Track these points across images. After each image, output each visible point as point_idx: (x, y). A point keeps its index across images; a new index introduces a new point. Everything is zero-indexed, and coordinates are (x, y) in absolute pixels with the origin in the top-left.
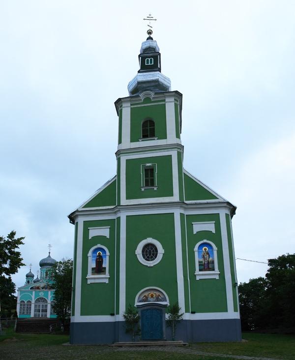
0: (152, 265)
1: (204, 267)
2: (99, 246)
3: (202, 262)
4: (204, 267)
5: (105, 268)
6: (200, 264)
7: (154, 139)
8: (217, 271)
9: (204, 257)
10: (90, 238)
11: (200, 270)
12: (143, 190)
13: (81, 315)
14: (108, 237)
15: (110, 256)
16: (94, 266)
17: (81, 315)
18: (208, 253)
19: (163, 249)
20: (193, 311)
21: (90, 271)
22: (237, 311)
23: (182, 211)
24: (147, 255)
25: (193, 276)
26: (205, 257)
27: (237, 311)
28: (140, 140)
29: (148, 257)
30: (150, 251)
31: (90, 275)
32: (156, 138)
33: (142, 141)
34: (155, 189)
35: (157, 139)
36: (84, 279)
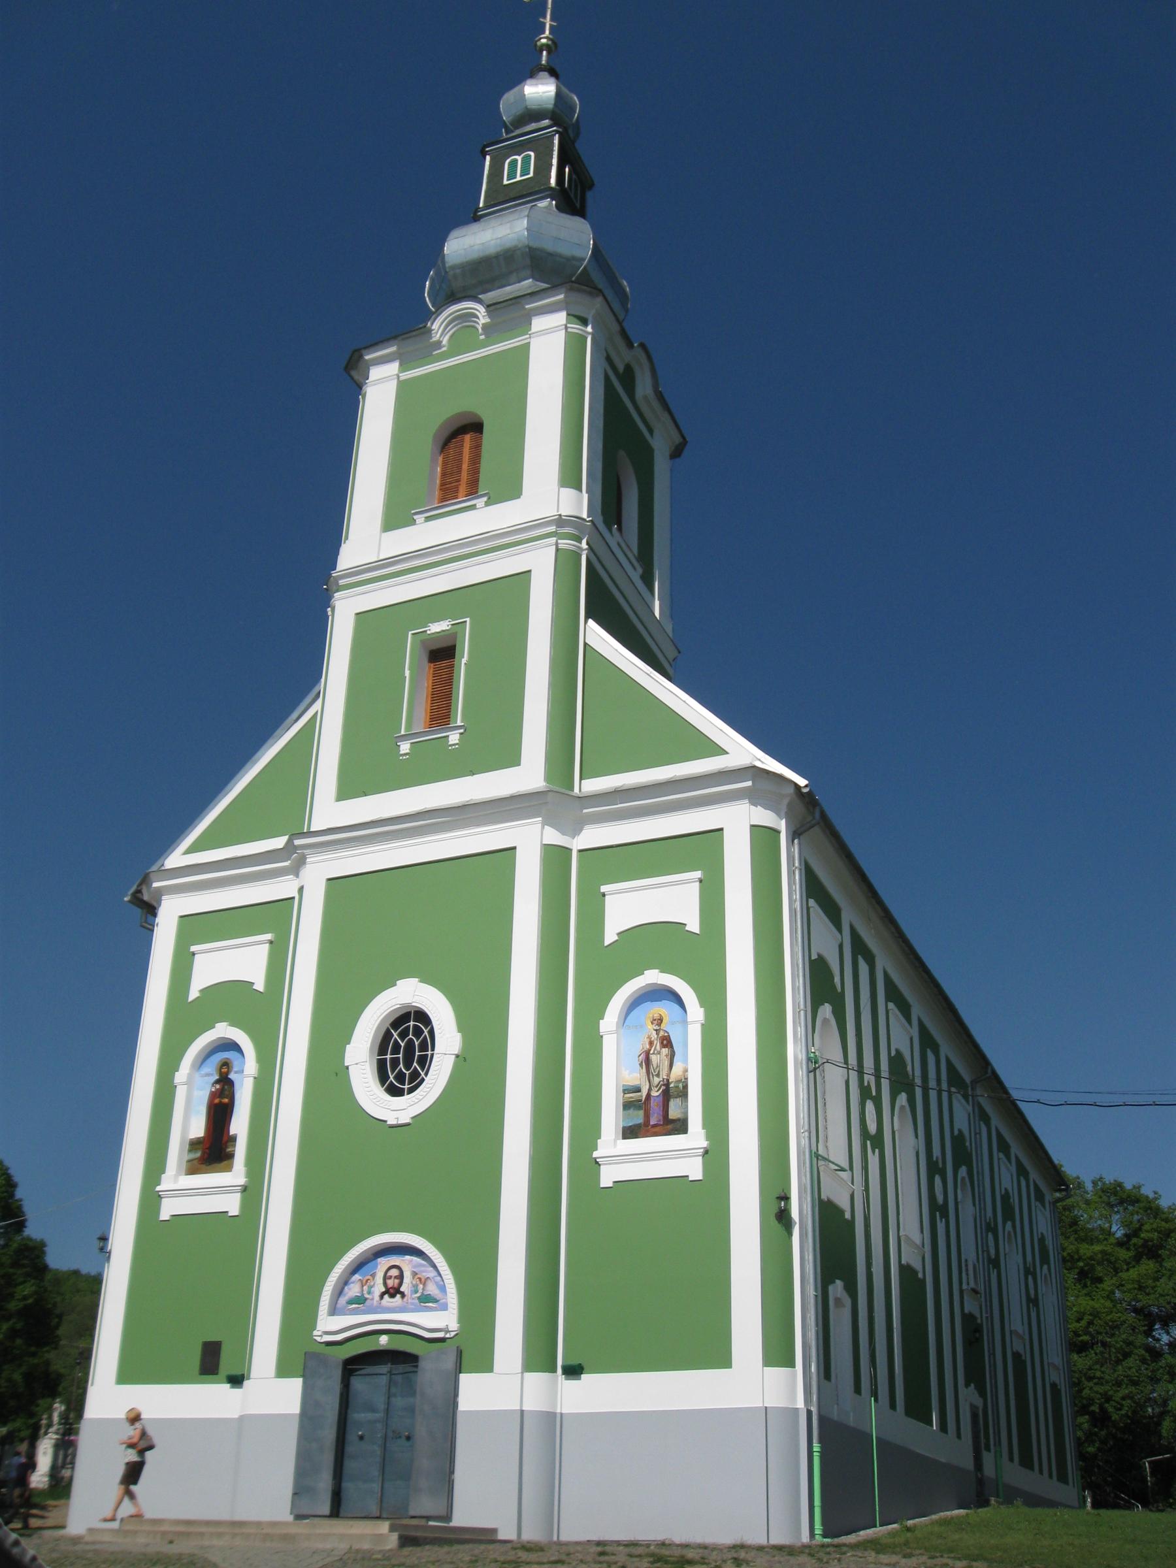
0: (405, 1118)
1: (647, 1116)
2: (653, 977)
3: (638, 1090)
4: (647, 1116)
5: (234, 1139)
6: (632, 1101)
7: (473, 507)
8: (696, 1137)
9: (647, 1061)
10: (610, 937)
11: (630, 1132)
12: (405, 747)
13: (731, 1367)
14: (260, 986)
15: (705, 1028)
16: (198, 1128)
17: (731, 1367)
18: (667, 1042)
19: (461, 1028)
20: (574, 1362)
21: (611, 1116)
22: (791, 1363)
23: (553, 836)
24: (395, 1062)
25: (588, 1166)
26: (654, 1059)
27: (791, 1363)
28: (420, 519)
29: (400, 1077)
30: (410, 1046)
31: (174, 1178)
32: (480, 502)
33: (428, 519)
34: (454, 738)
35: (487, 504)
36: (150, 1199)
